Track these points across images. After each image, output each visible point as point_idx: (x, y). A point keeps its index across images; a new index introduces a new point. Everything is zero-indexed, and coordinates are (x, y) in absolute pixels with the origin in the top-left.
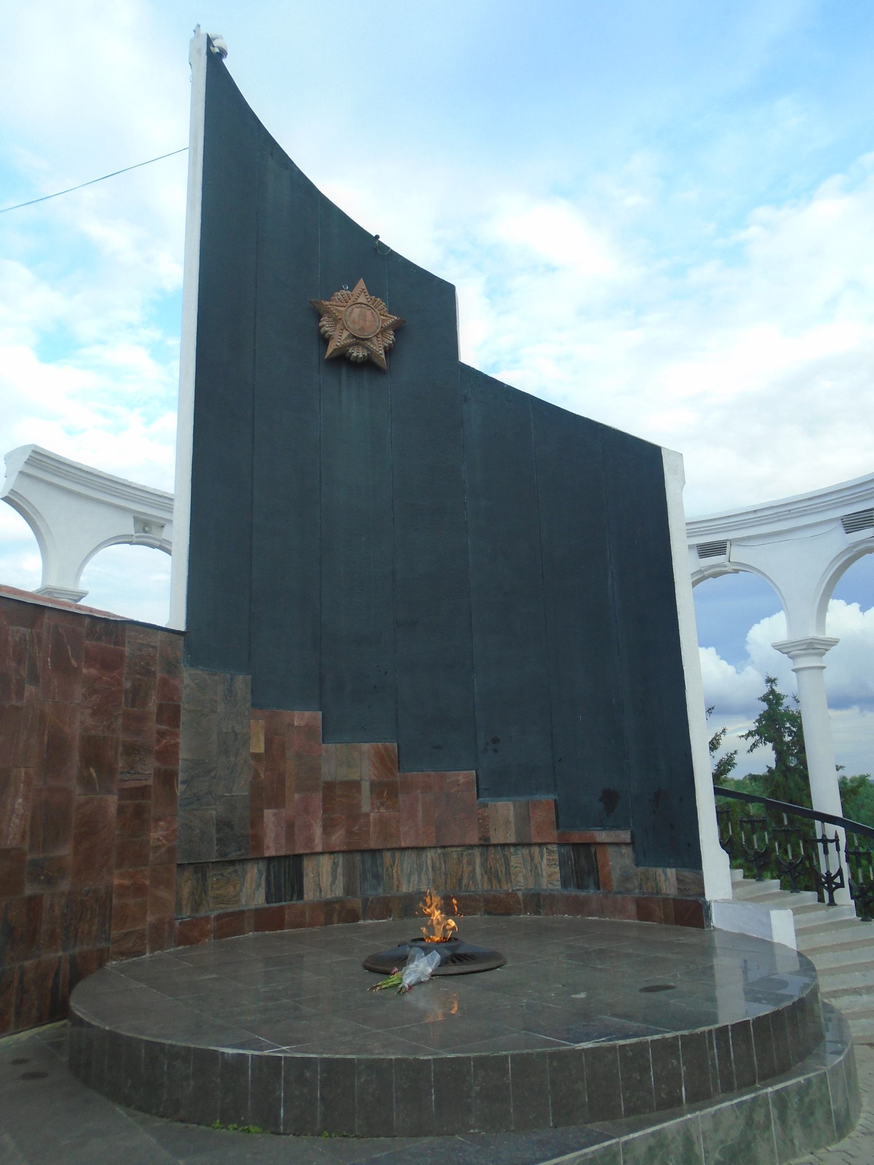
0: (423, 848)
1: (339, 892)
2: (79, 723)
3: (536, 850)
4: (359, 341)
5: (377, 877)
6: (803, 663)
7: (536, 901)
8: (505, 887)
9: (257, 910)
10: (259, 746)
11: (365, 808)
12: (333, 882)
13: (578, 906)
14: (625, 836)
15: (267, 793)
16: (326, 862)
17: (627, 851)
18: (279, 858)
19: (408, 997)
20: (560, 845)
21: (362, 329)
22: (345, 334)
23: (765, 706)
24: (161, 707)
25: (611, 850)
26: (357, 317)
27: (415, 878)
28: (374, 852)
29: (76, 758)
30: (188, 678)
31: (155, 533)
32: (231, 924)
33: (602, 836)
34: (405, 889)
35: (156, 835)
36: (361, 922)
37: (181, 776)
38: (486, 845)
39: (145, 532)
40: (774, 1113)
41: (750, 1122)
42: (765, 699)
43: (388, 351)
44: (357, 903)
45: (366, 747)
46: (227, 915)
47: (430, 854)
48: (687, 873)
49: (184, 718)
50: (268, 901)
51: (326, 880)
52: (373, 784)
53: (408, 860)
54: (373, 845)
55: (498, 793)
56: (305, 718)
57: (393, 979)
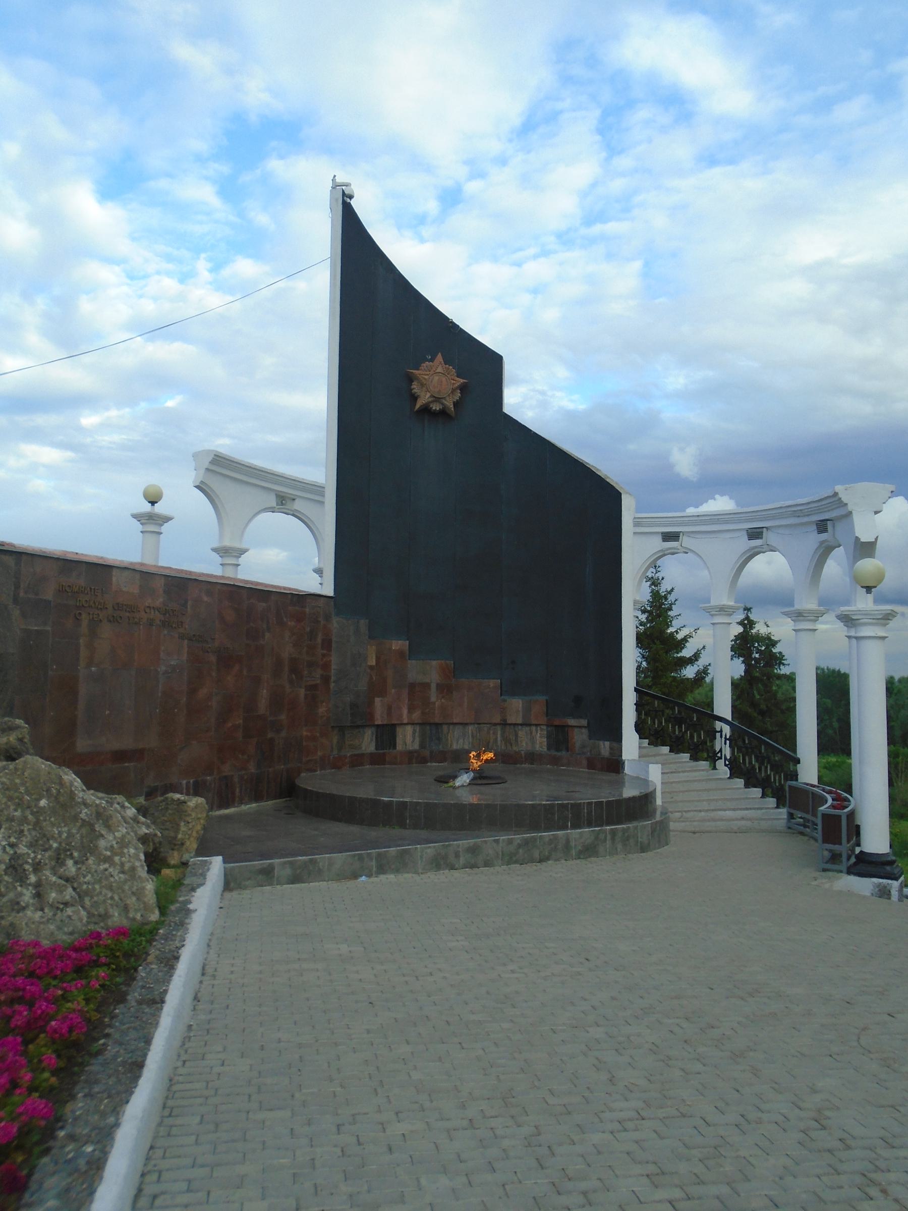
0: (467, 724)
1: (416, 746)
2: (288, 651)
3: (534, 728)
4: (437, 400)
5: (439, 739)
6: (717, 620)
7: (532, 757)
8: (515, 748)
9: (371, 754)
10: (372, 662)
11: (433, 699)
12: (413, 741)
13: (555, 761)
14: (584, 722)
15: (377, 689)
16: (409, 729)
17: (584, 731)
18: (383, 725)
19: (457, 791)
20: (547, 726)
21: (439, 392)
22: (428, 395)
23: (740, 629)
24: (323, 640)
25: (576, 730)
26: (437, 381)
27: (461, 741)
28: (437, 725)
29: (286, 669)
30: (335, 623)
31: (289, 505)
32: (357, 760)
33: (572, 722)
34: (455, 747)
35: (322, 710)
36: (429, 764)
37: (333, 679)
38: (504, 724)
39: (282, 504)
40: (609, 837)
41: (597, 838)
42: (741, 623)
43: (456, 404)
44: (427, 753)
45: (434, 663)
46: (355, 755)
47: (470, 728)
48: (615, 745)
49: (334, 645)
50: (376, 749)
51: (409, 739)
52: (438, 685)
53: (457, 731)
54: (437, 720)
55: (513, 694)
56: (398, 644)
57: (451, 784)
